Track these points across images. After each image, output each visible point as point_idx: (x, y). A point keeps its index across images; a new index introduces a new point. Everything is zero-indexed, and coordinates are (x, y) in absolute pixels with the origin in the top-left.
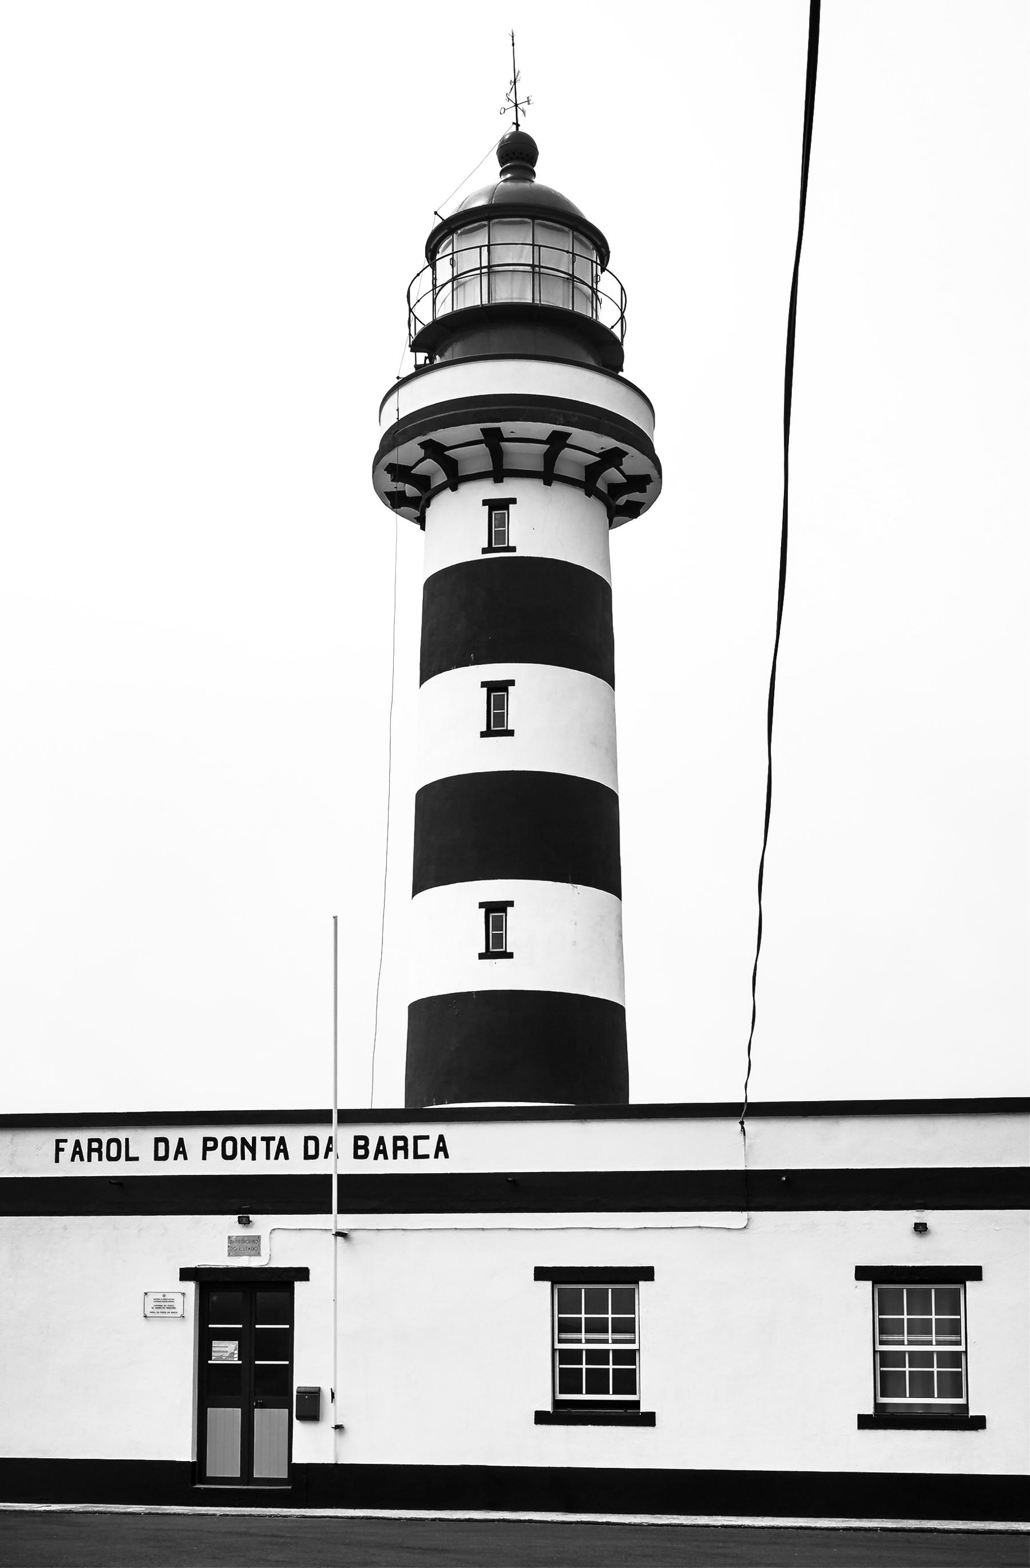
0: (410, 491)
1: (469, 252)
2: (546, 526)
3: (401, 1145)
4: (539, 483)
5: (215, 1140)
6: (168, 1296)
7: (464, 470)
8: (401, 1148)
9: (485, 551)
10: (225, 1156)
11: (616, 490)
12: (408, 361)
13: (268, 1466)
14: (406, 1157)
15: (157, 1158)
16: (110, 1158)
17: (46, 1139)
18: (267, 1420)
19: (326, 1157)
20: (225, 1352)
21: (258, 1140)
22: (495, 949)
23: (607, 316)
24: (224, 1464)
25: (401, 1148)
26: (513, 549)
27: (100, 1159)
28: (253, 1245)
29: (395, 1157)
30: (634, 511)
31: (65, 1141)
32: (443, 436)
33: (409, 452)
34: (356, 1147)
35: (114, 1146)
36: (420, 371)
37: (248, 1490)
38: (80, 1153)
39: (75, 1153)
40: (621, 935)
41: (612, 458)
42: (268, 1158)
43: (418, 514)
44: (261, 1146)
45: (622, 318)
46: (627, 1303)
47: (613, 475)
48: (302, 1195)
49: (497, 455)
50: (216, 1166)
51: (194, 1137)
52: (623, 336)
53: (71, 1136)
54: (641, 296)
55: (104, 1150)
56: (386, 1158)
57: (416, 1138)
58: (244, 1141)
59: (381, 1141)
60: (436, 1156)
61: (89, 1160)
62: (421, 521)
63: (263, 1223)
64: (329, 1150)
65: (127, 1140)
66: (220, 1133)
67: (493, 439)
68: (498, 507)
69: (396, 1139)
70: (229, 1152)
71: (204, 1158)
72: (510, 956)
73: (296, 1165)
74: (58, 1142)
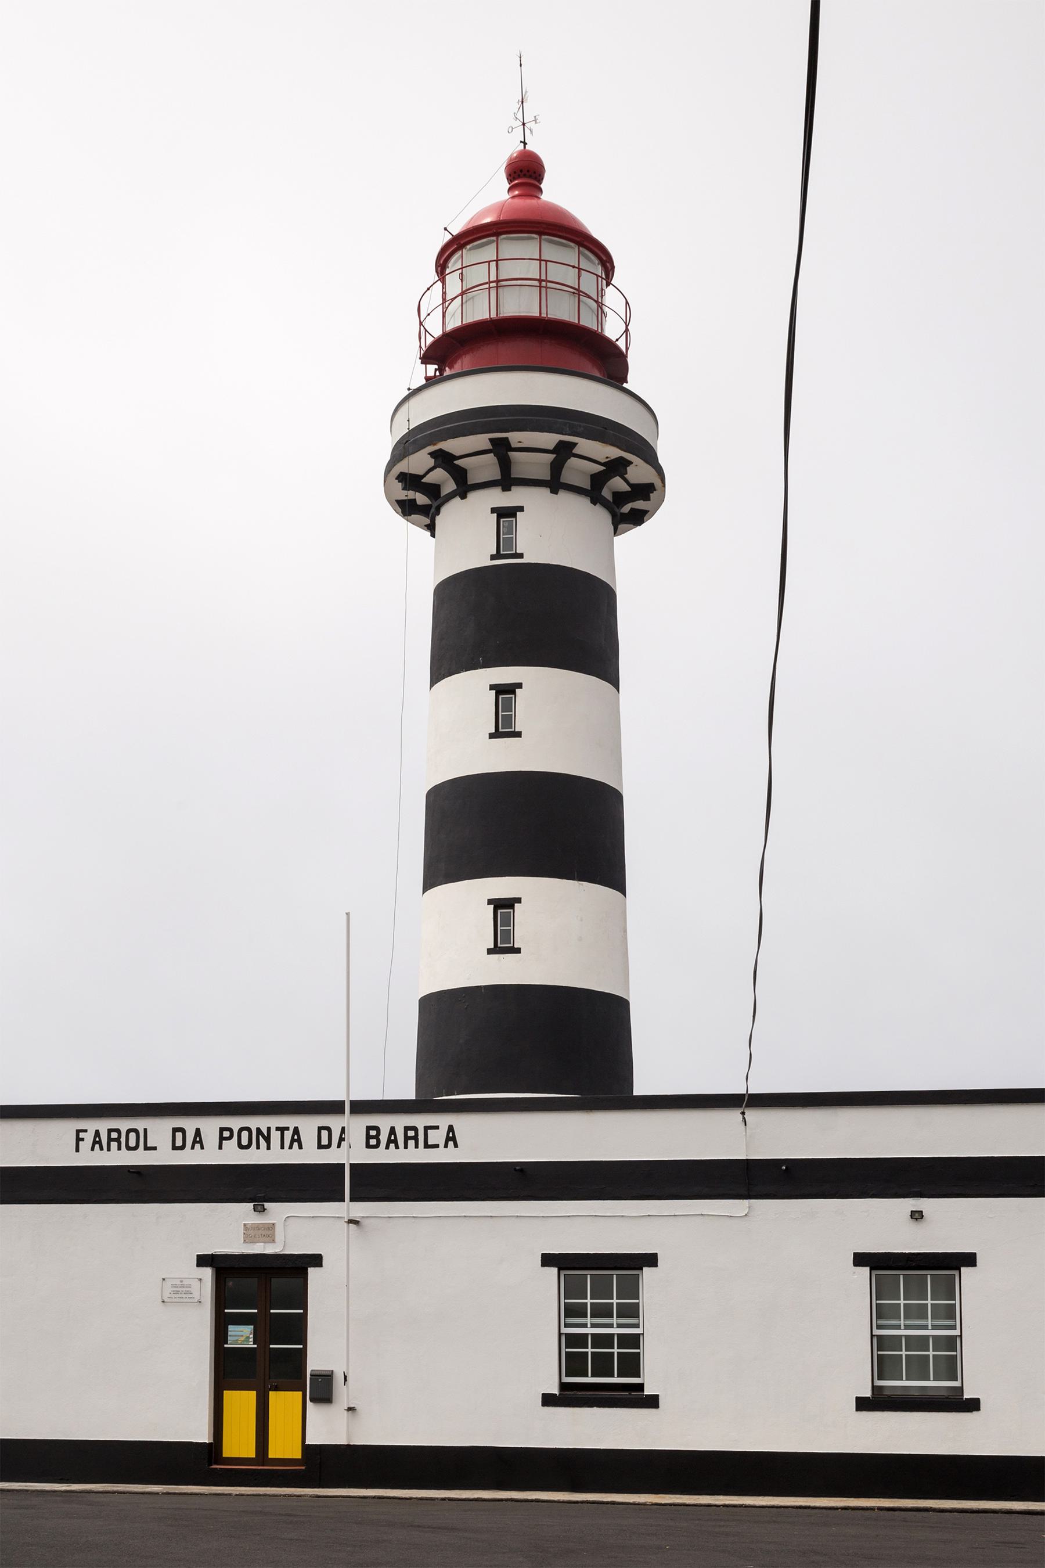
0: (421, 499)
2: (553, 532)
4: (545, 492)
5: (230, 1130)
6: (186, 1282)
8: (411, 1138)
9: (493, 557)
11: (620, 498)
13: (284, 1446)
14: (417, 1146)
15: (320, 1146)
16: (128, 1148)
18: (284, 1404)
19: (339, 1146)
20: (241, 1336)
21: (273, 1130)
22: (503, 945)
23: (612, 330)
24: (240, 1444)
25: (411, 1138)
26: (521, 556)
27: (119, 1148)
28: (268, 1232)
29: (406, 1147)
30: (638, 518)
31: (86, 1131)
32: (454, 446)
33: (419, 462)
34: (368, 1137)
36: (430, 382)
37: (262, 1470)
38: (100, 1143)
39: (95, 1143)
40: (625, 931)
41: (617, 467)
42: (282, 1147)
43: (428, 521)
44: (275, 1136)
45: (627, 331)
46: (631, 1289)
47: (617, 484)
48: (315, 1184)
49: (505, 464)
50: (232, 1155)
51: (210, 1126)
52: (627, 349)
53: (92, 1125)
54: (636, 309)
55: (123, 1140)
56: (397, 1147)
58: (259, 1130)
59: (393, 1131)
60: (446, 1146)
61: (109, 1149)
62: (431, 528)
63: (278, 1211)
64: (341, 1139)
65: (145, 1130)
66: (235, 1123)
67: (501, 449)
69: (407, 1129)
70: (245, 1142)
71: (220, 1148)
72: (518, 951)
74: (78, 1132)
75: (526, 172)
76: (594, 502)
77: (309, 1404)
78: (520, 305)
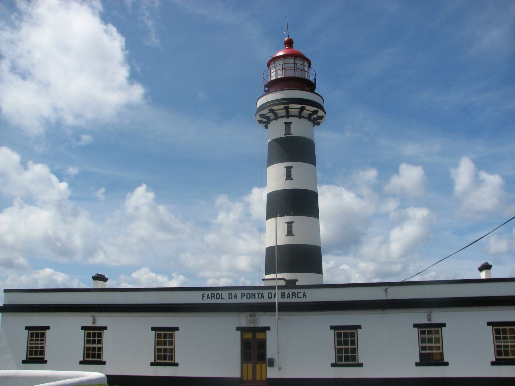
1: (279, 64)
2: (300, 128)
3: (294, 295)
4: (297, 119)
5: (244, 294)
7: (279, 115)
10: (247, 298)
11: (315, 119)
12: (263, 89)
15: (229, 298)
17: (201, 293)
23: (311, 79)
30: (318, 124)
33: (265, 112)
34: (282, 295)
35: (218, 295)
38: (289, 296)
41: (315, 112)
44: (257, 295)
47: (315, 116)
48: (268, 308)
49: (287, 112)
50: (245, 300)
51: (239, 293)
53: (207, 293)
54: (316, 74)
55: (296, 296)
57: (298, 293)
58: (252, 294)
59: (289, 293)
62: (267, 127)
64: (275, 296)
67: (287, 108)
68: (288, 125)
69: (292, 293)
70: (248, 297)
73: (266, 300)
75: (289, 43)
76: (309, 120)
77: (267, 367)
78: (291, 74)
